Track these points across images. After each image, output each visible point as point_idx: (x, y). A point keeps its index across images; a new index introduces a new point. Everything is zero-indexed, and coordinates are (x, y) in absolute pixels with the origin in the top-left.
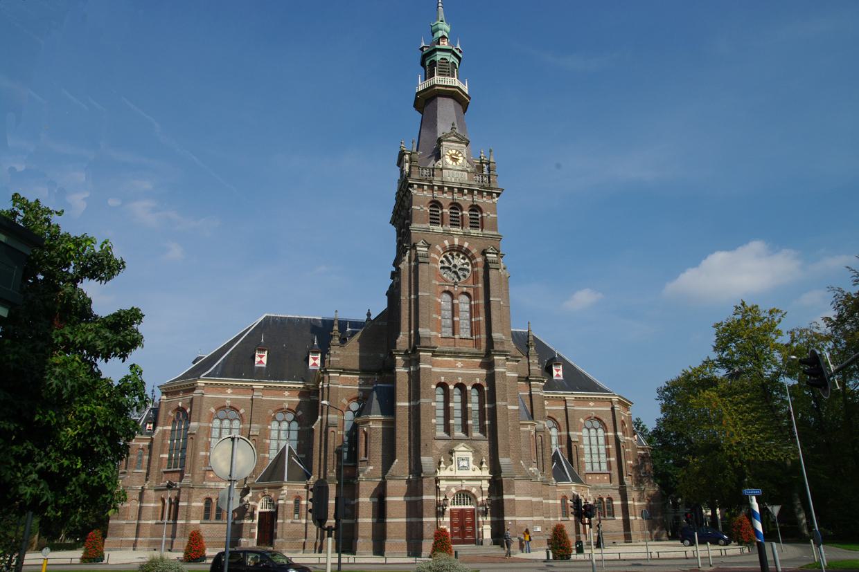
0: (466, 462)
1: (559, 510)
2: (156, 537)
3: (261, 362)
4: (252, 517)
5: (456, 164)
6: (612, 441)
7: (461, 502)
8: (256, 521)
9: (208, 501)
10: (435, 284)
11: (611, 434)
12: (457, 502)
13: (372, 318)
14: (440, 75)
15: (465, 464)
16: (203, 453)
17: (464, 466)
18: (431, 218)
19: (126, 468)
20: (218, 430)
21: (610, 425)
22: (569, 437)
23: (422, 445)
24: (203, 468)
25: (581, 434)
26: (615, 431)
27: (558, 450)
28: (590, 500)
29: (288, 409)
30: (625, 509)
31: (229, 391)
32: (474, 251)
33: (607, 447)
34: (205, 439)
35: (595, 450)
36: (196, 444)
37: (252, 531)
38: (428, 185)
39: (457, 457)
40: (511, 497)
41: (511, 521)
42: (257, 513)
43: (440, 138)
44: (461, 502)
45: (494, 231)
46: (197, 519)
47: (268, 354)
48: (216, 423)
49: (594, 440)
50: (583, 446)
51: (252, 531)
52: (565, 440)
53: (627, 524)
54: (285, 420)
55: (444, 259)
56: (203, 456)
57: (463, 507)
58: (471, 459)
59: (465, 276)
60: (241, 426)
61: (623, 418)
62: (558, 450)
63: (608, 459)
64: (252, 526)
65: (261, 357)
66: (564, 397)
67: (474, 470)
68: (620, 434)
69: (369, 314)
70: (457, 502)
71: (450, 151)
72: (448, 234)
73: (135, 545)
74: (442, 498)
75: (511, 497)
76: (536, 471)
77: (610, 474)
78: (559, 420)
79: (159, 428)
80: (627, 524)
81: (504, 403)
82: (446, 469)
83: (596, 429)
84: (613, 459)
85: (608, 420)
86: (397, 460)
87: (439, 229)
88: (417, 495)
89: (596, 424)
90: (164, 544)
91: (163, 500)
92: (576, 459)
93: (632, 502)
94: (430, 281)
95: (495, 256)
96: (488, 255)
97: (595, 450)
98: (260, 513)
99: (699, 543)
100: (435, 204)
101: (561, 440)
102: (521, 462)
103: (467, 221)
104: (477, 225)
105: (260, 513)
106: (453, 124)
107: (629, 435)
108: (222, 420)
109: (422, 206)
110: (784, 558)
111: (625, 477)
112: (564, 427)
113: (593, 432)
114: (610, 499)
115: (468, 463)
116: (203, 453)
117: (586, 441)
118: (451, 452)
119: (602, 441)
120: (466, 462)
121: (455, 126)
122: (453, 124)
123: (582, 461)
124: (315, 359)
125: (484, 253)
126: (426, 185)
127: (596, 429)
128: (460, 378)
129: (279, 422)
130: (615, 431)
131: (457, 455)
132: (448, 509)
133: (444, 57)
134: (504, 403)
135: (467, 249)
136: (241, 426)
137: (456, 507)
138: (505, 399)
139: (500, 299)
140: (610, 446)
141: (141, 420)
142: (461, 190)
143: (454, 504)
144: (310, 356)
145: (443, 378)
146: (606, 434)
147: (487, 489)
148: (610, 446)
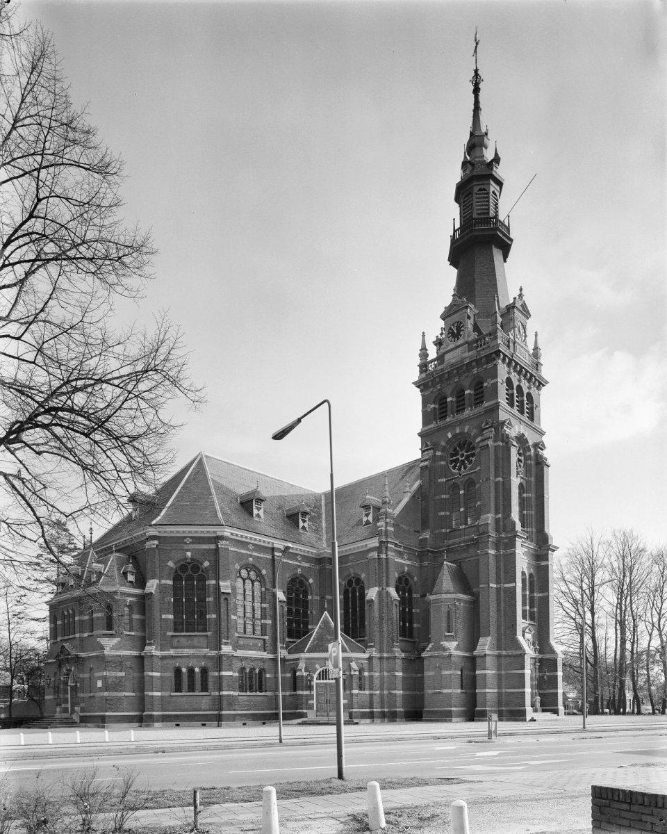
4: (310, 688)
8: (314, 692)
37: (310, 702)
51: (310, 702)
64: (311, 697)
65: (367, 515)
66: (273, 544)
133: (483, 187)
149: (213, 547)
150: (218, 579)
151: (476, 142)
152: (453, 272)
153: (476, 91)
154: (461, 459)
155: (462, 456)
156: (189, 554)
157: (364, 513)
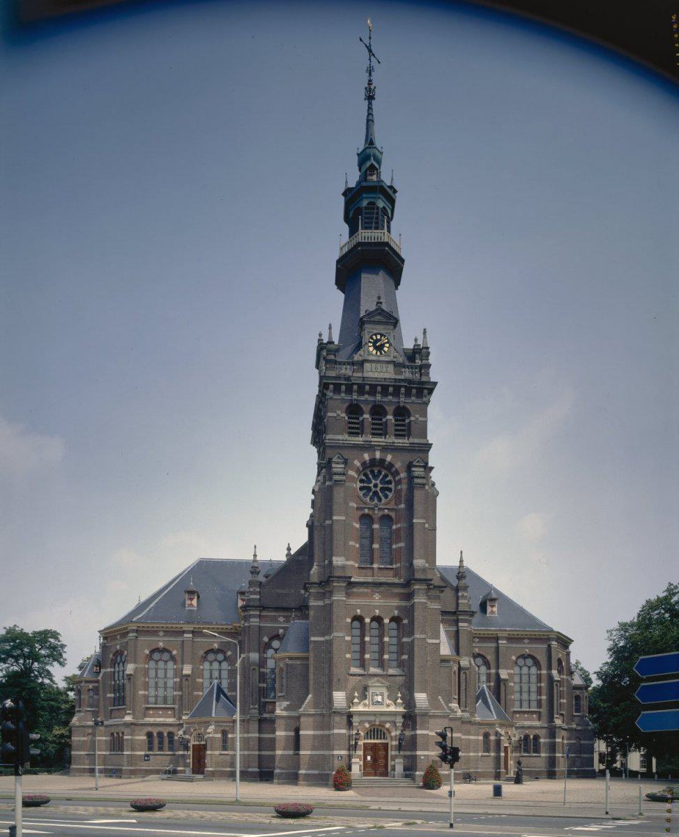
0: (380, 697)
1: (481, 744)
2: (111, 765)
3: (191, 605)
4: (187, 748)
5: (381, 353)
6: (544, 678)
7: (374, 736)
9: (149, 735)
10: (352, 507)
11: (544, 672)
12: (371, 736)
13: (293, 552)
14: (366, 228)
15: (379, 699)
16: (141, 692)
17: (378, 702)
18: (349, 428)
19: (80, 707)
20: (163, 671)
21: (544, 663)
22: (498, 675)
23: (335, 679)
24: (143, 706)
25: (512, 672)
26: (550, 668)
27: (485, 688)
28: (515, 736)
29: (218, 649)
30: (552, 748)
31: (526, 641)
32: (398, 465)
33: (538, 685)
34: (143, 679)
35: (525, 688)
36: (134, 684)
38: (345, 384)
39: (371, 692)
40: (425, 732)
41: (423, 755)
42: (190, 745)
43: (361, 319)
44: (374, 736)
45: (422, 438)
46: (141, 750)
47: (198, 597)
48: (207, 665)
49: (161, 674)
50: (512, 684)
52: (493, 678)
53: (552, 762)
54: (216, 660)
55: (364, 478)
56: (142, 695)
57: (376, 741)
58: (386, 694)
59: (386, 497)
60: (175, 667)
61: (560, 655)
62: (485, 688)
63: (538, 697)
65: (191, 599)
67: (388, 706)
68: (554, 672)
69: (289, 549)
70: (371, 736)
71: (374, 337)
72: (369, 447)
73: (92, 771)
74: (354, 732)
75: (425, 732)
76: (456, 707)
77: (540, 712)
78: (489, 657)
79: (103, 671)
80: (552, 762)
81: (423, 636)
82: (359, 703)
83: (529, 667)
84: (544, 697)
85: (542, 658)
86: (310, 696)
87: (359, 440)
88: (412, 750)
89: (529, 662)
90: (453, 778)
91: (112, 734)
92: (504, 695)
93: (560, 740)
94: (346, 503)
95: (422, 469)
96: (413, 469)
97: (525, 688)
98: (193, 745)
99: (241, 780)
100: (354, 410)
101: (490, 678)
102: (440, 697)
103: (391, 429)
104: (403, 433)
105: (193, 745)
106: (379, 298)
107: (565, 672)
108: (211, 663)
109: (339, 412)
110: (257, 748)
111: (555, 716)
112: (493, 664)
113: (161, 664)
114: (536, 738)
115: (383, 699)
116: (141, 692)
117: (206, 674)
118: (366, 688)
119: (534, 679)
120: (380, 697)
121: (381, 300)
122: (379, 298)
123: (510, 700)
124: (492, 606)
125: (410, 467)
126: (343, 384)
127: (529, 667)
128: (358, 611)
129: (157, 661)
130: (550, 668)
131: (371, 690)
132: (361, 743)
134: (423, 636)
135: (389, 463)
136: (175, 667)
137: (369, 741)
138: (423, 632)
139: (423, 521)
140: (543, 685)
141: (88, 664)
142: (385, 389)
143: (367, 739)
144: (239, 597)
145: (377, 611)
146: (539, 672)
147: (401, 724)
148: (543, 685)
149: (494, 645)
150: (498, 668)
151: (368, 160)
152: (340, 296)
153: (370, 98)
154: (371, 485)
155: (376, 486)
156: (118, 647)
157: (187, 596)
